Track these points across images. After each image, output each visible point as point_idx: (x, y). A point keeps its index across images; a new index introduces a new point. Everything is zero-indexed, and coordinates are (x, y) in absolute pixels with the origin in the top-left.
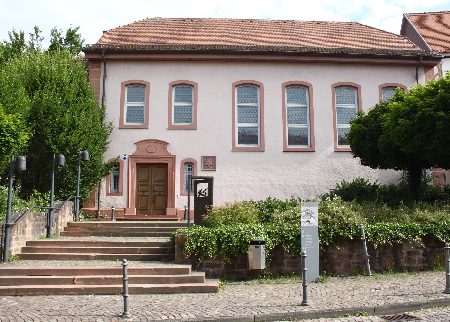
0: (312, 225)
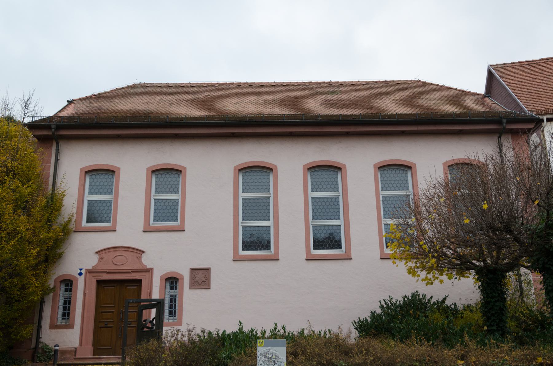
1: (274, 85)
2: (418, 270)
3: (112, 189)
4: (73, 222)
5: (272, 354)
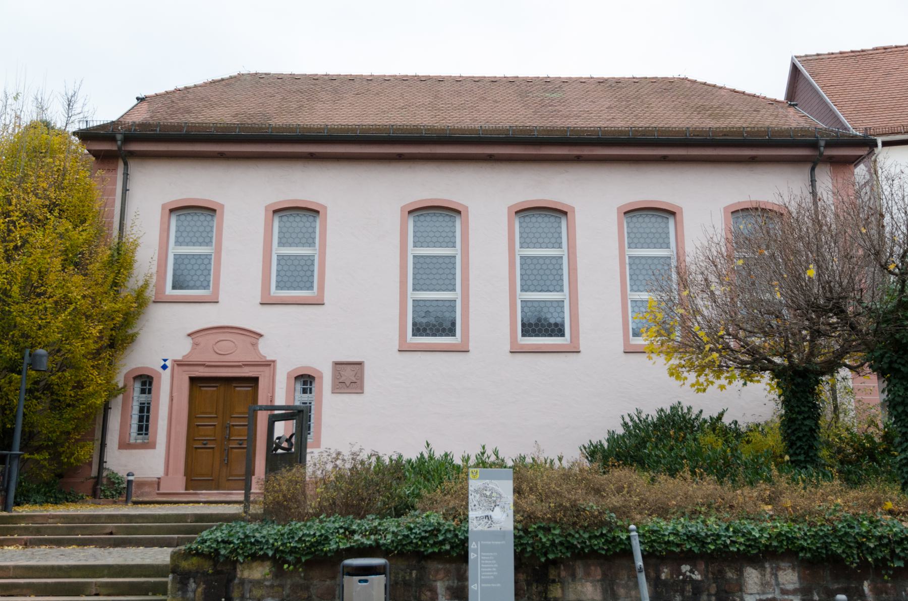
0: (496, 527)
1: (459, 81)
2: (684, 369)
3: (211, 238)
4: (151, 286)
5: (492, 490)
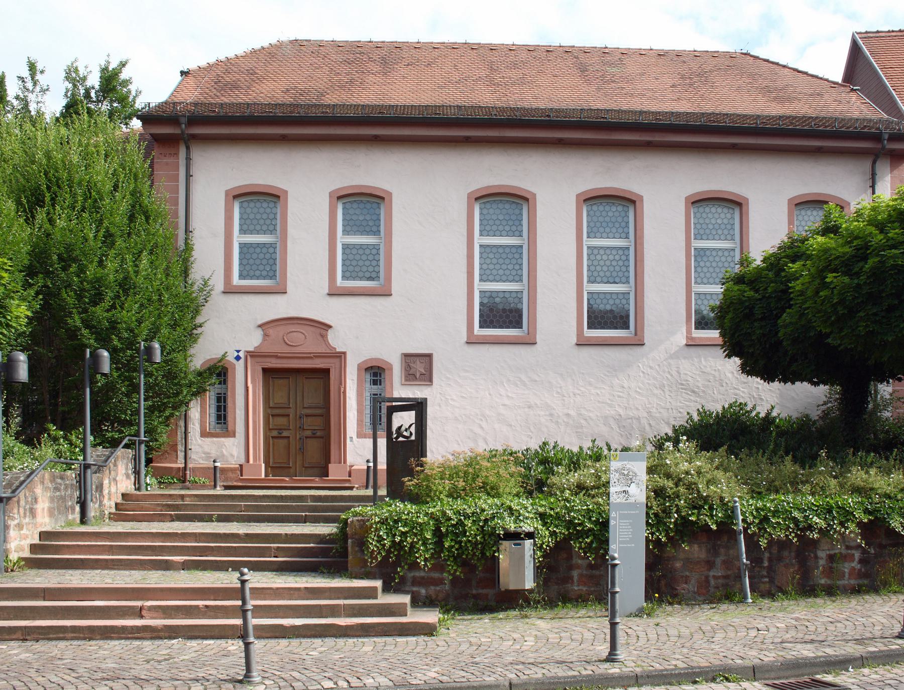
3: (275, 225)
